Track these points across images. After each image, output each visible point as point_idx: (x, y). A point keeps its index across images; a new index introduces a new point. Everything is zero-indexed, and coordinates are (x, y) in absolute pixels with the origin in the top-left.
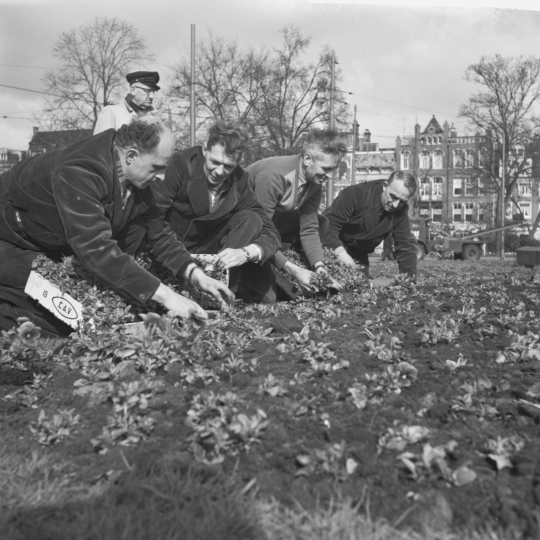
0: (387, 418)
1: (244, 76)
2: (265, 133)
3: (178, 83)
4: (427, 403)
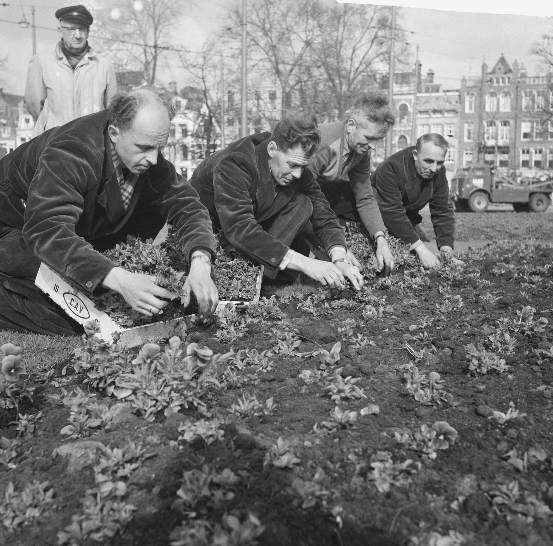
0: (411, 518)
1: (300, 15)
2: (321, 75)
3: (231, 23)
4: (463, 489)
